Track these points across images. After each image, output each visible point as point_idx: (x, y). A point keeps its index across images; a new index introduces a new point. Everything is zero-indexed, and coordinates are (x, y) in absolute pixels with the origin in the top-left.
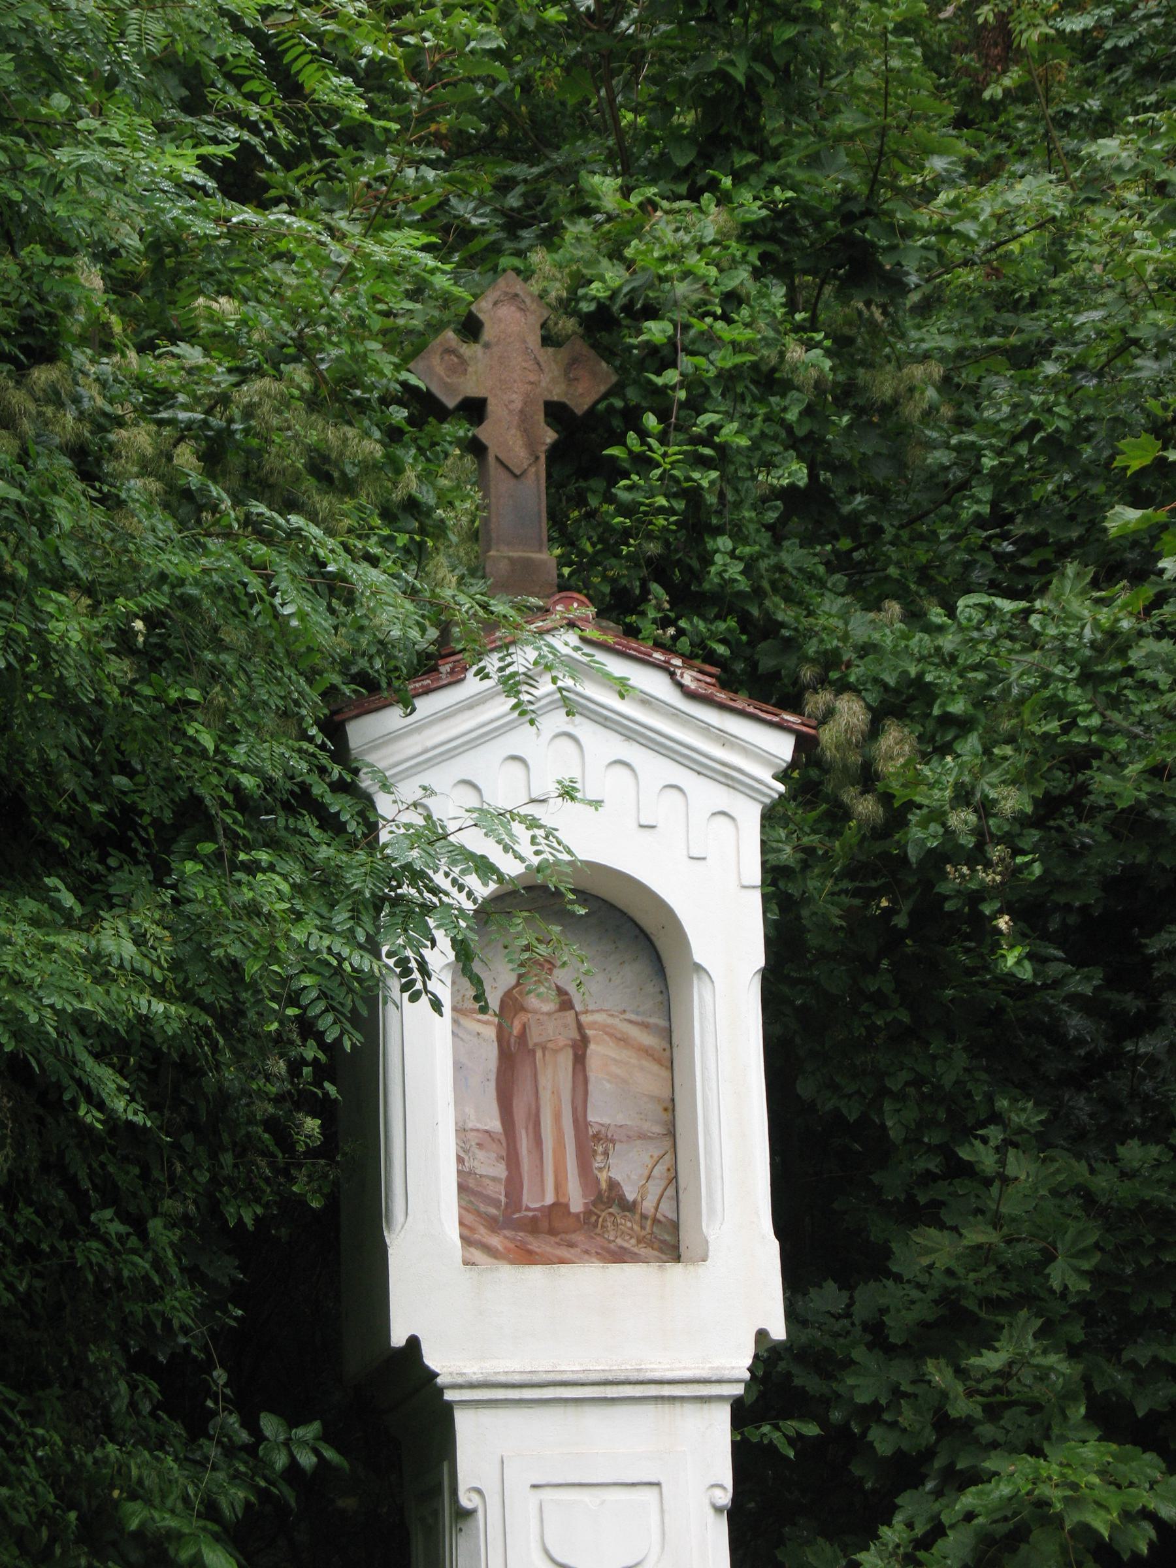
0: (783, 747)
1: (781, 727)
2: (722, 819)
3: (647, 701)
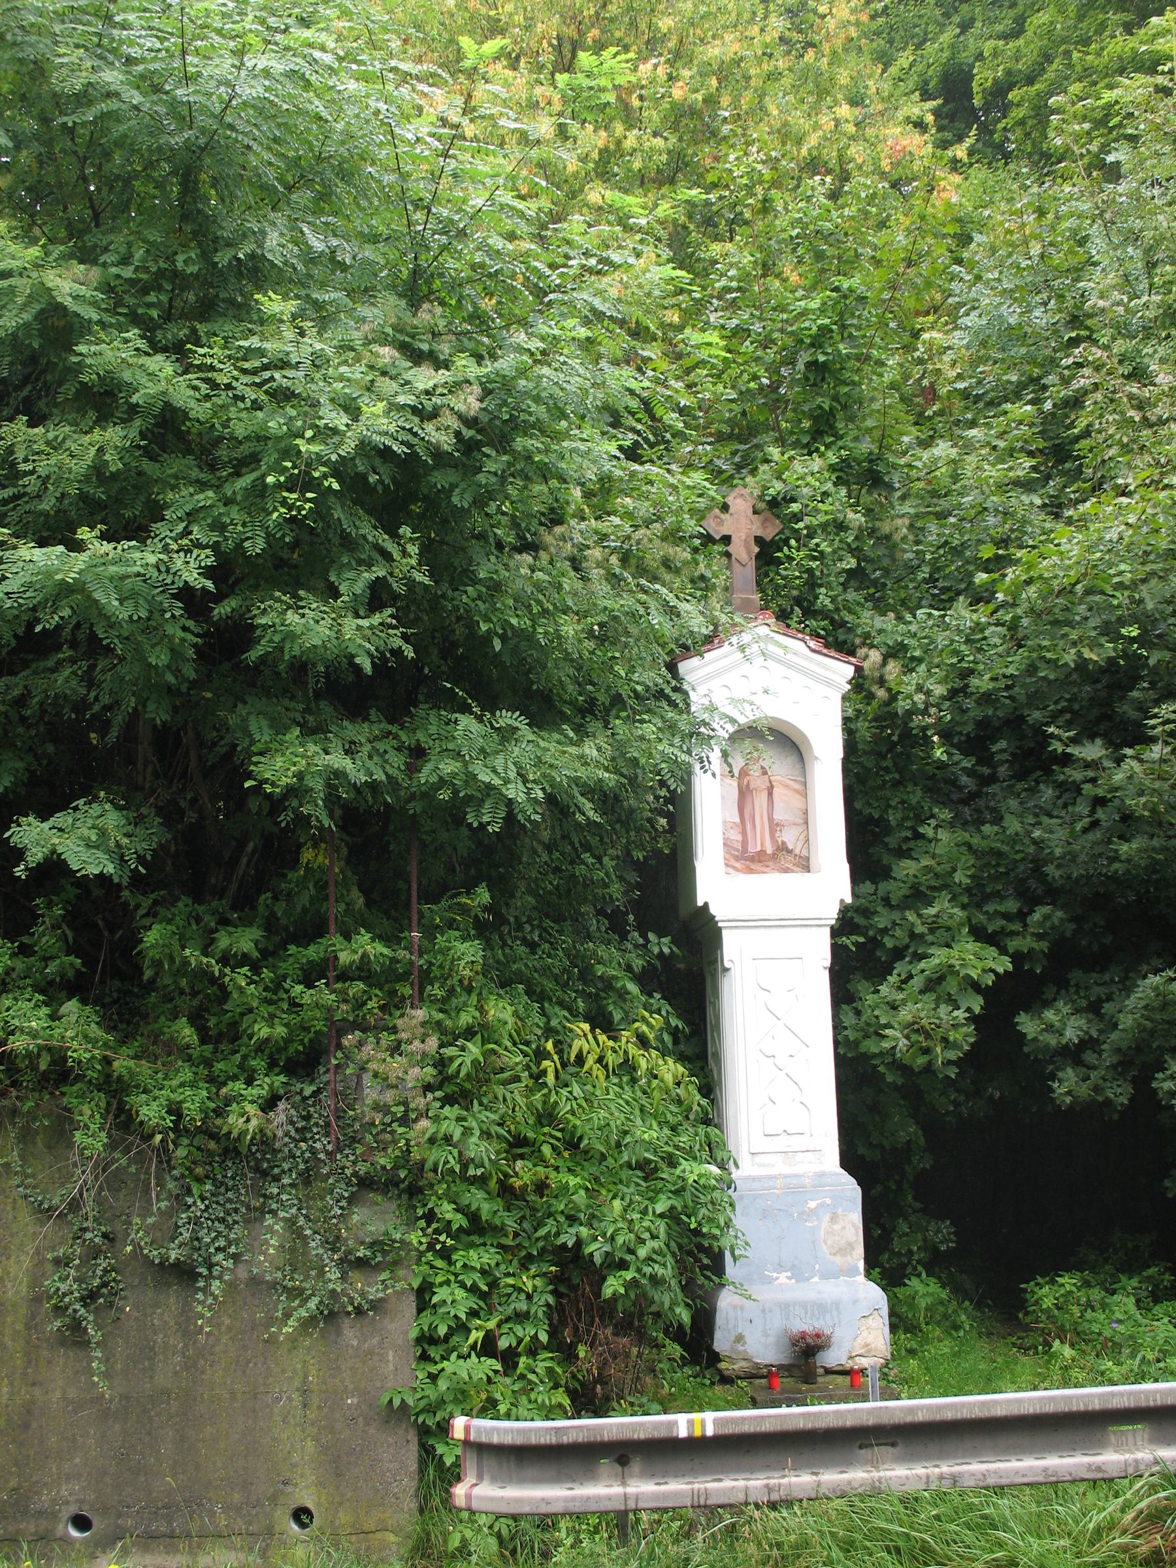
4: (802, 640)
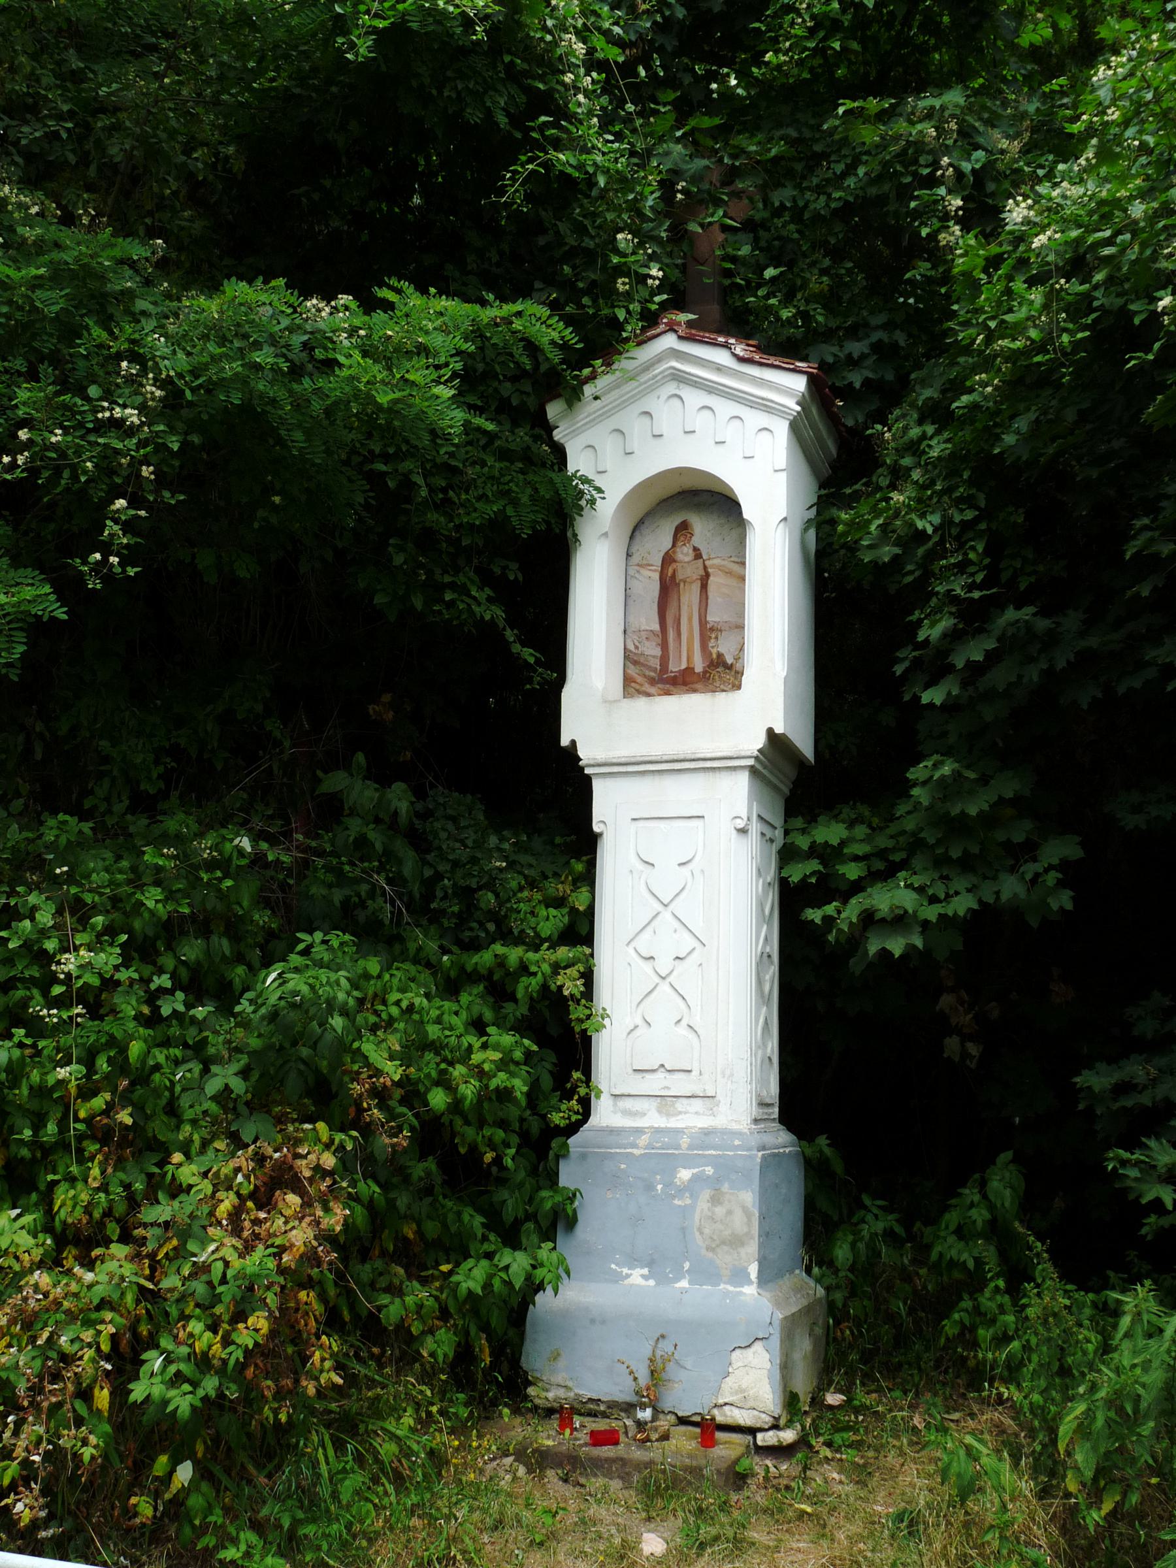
0: (799, 383)
1: (796, 371)
2: (765, 433)
3: (719, 369)
4: (726, 346)
